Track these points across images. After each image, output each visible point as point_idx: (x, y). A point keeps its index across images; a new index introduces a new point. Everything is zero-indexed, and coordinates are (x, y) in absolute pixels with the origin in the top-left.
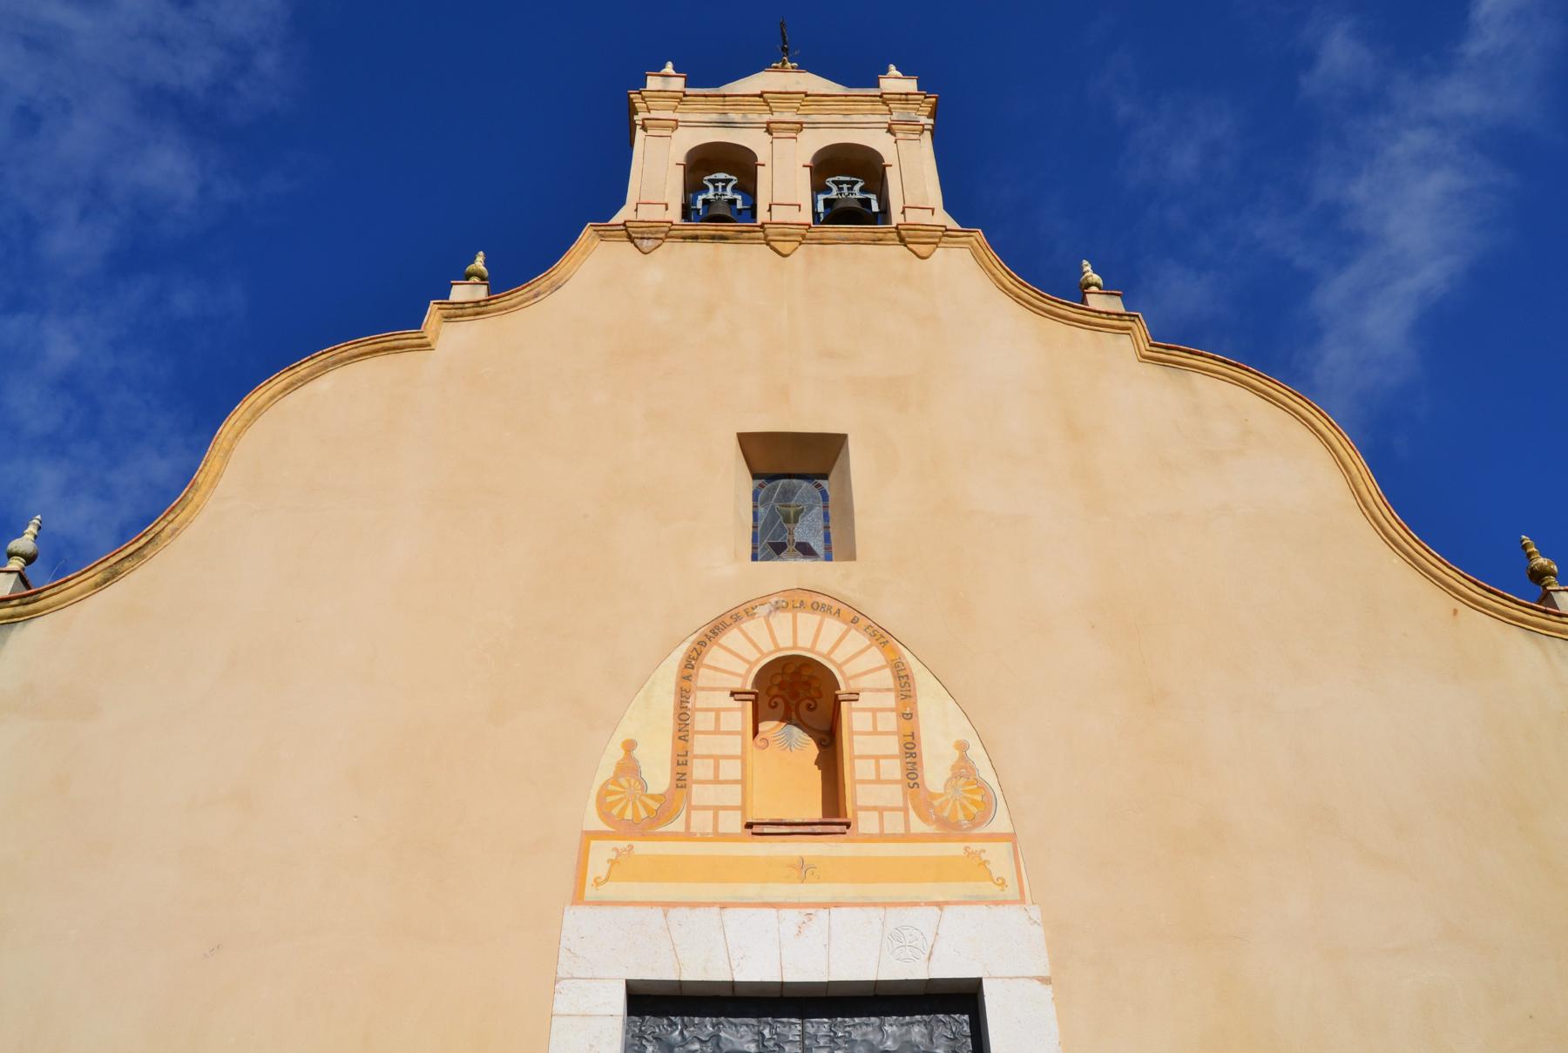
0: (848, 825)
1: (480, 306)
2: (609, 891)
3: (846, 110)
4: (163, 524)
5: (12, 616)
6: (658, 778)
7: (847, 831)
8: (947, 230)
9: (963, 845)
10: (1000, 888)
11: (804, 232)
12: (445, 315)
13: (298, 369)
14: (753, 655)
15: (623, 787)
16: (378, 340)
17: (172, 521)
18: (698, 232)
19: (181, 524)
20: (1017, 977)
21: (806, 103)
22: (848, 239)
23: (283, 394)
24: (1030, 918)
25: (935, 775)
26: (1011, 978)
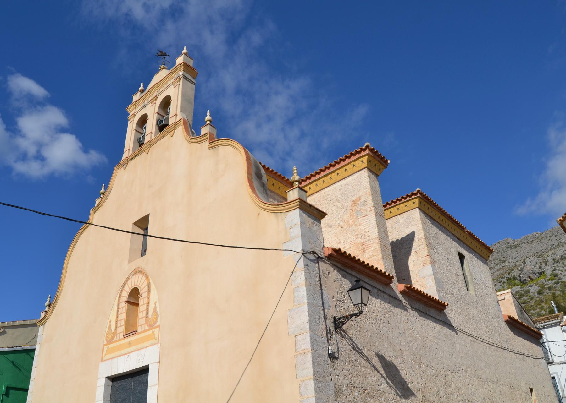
0: (136, 331)
8: (175, 123)
9: (152, 331)
19: (61, 291)
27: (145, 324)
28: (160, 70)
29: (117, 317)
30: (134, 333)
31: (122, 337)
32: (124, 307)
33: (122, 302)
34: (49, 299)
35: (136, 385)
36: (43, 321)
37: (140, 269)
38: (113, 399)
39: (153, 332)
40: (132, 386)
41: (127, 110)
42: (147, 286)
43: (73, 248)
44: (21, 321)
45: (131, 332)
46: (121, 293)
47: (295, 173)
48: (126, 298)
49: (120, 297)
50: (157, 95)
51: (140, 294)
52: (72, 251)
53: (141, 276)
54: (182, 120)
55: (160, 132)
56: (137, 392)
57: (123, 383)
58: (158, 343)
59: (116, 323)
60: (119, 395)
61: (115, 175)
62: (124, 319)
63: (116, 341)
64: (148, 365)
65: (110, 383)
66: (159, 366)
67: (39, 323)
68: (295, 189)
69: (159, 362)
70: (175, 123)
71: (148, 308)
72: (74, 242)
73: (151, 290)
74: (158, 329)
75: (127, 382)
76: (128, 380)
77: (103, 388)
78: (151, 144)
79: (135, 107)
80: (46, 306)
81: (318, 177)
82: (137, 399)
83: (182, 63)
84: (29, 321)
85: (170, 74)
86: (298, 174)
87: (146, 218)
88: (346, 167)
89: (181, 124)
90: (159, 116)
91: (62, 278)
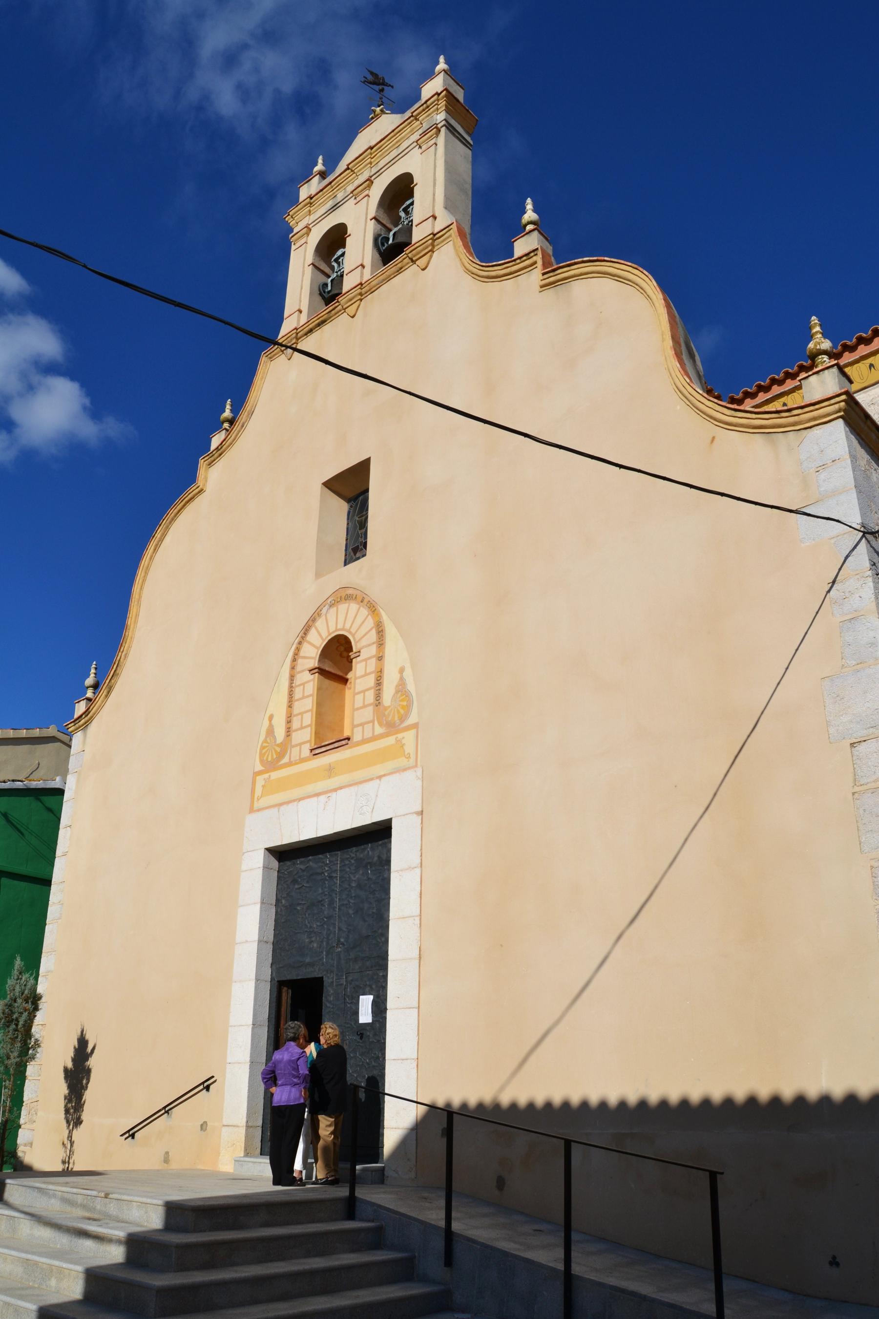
1: (219, 450)
2: (263, 802)
3: (397, 142)
4: (120, 654)
5: (86, 723)
6: (280, 734)
7: (349, 742)
8: (434, 235)
9: (394, 737)
10: (407, 760)
11: (359, 291)
12: (208, 464)
13: (156, 535)
14: (358, 636)
15: (268, 743)
16: (184, 497)
17: (123, 651)
18: (311, 326)
20: (407, 814)
21: (434, 104)
22: (384, 280)
23: (155, 553)
24: (417, 776)
25: (387, 697)
26: (404, 815)
27: (373, 722)
28: (372, 118)
29: (290, 706)
30: (343, 742)
31: (306, 752)
32: (309, 683)
33: (303, 671)
34: (93, 671)
35: (349, 868)
36: (83, 721)
37: (350, 592)
38: (283, 901)
39: (398, 741)
40: (337, 870)
41: (286, 219)
42: (374, 632)
43: (155, 550)
44: (8, 730)
45: (334, 741)
46: (298, 649)
47: (817, 332)
48: (313, 661)
49: (294, 660)
50: (371, 177)
51: (354, 650)
52: (151, 558)
53: (354, 606)
54: (454, 226)
55: (385, 265)
56: (354, 885)
57: (311, 863)
58: (416, 766)
59: (289, 722)
60: (300, 893)
61: (264, 373)
62: (311, 710)
63: (290, 764)
64: (391, 819)
65: (275, 864)
66: (422, 823)
67: (73, 724)
68: (826, 371)
69: (422, 811)
70: (434, 235)
71: (379, 683)
72: (158, 535)
73: (387, 641)
74: (413, 732)
75: (323, 862)
76: (327, 858)
77: (259, 874)
78: (364, 291)
79: (310, 211)
80: (88, 688)
81: (793, 386)
82: (352, 901)
83: (442, 92)
84: (25, 730)
85: (409, 121)
86: (825, 335)
87: (362, 470)
88: (872, 358)
89: (450, 236)
90: (379, 227)
91: (130, 621)
